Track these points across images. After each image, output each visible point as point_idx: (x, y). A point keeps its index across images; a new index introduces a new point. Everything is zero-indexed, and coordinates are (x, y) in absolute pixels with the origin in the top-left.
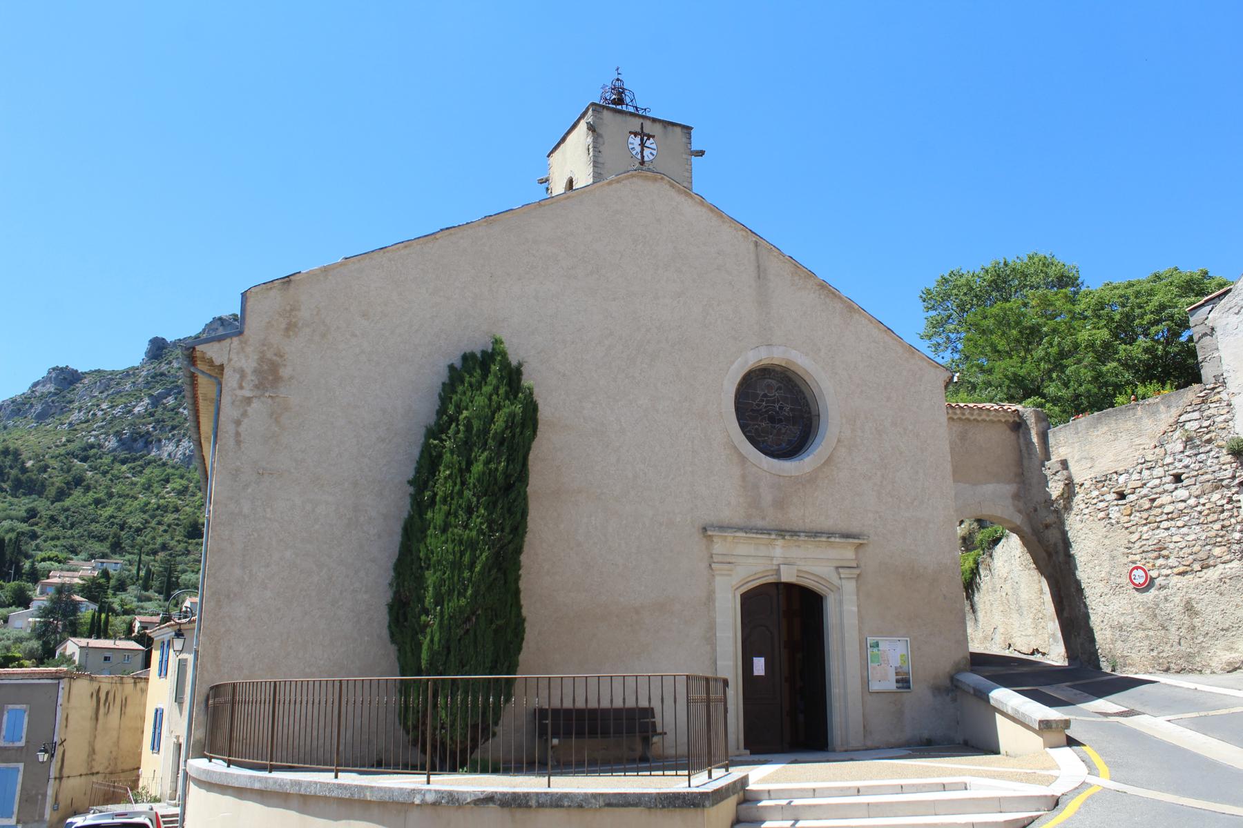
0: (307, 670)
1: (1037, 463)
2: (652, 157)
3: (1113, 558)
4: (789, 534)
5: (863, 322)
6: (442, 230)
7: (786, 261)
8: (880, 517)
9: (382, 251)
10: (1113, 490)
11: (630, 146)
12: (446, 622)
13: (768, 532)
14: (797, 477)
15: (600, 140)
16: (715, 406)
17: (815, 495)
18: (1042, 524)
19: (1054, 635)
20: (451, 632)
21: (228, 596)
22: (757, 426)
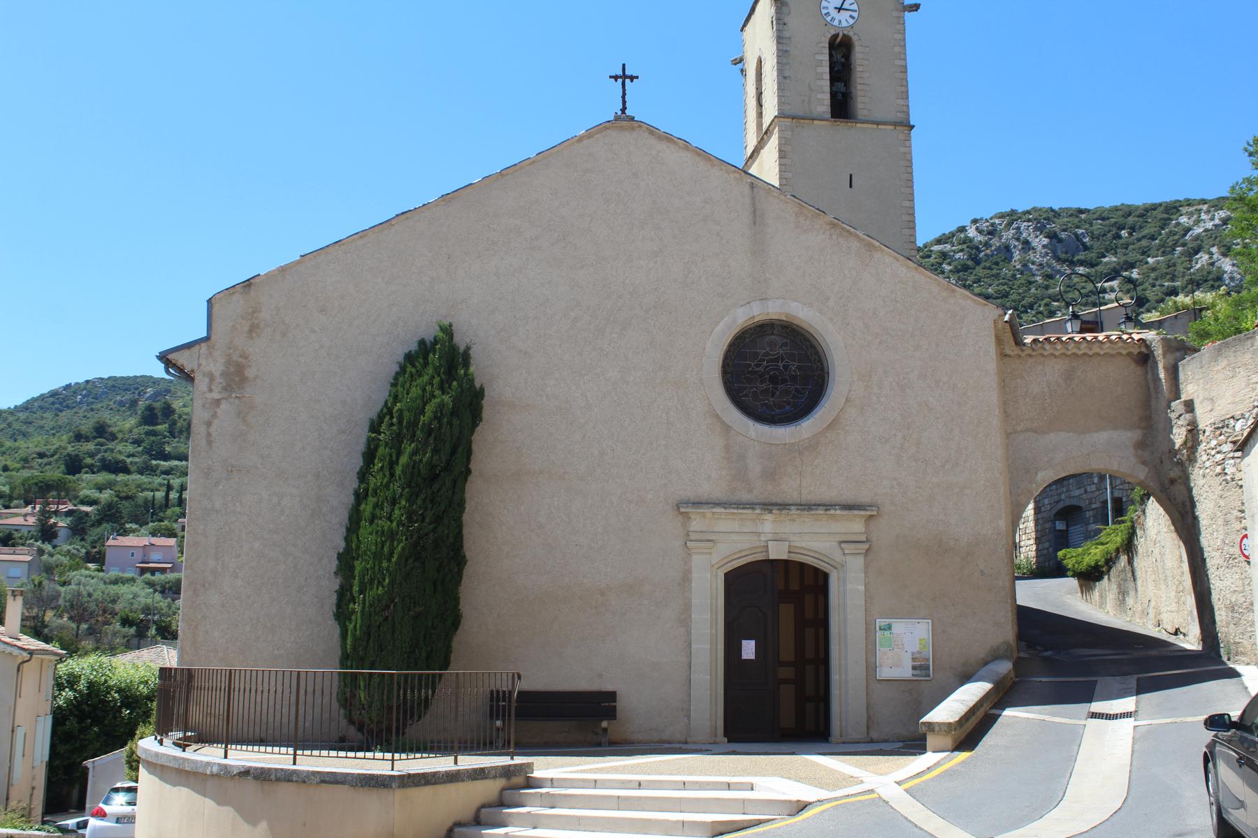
0: (276, 652)
1: (1164, 404)
2: (851, 21)
3: (1227, 523)
4: (778, 507)
5: (887, 260)
6: (397, 215)
7: (788, 200)
8: (899, 484)
9: (337, 245)
10: (1230, 439)
11: (824, 11)
12: (367, 609)
13: (751, 505)
14: (793, 445)
15: (785, 10)
16: (695, 373)
17: (815, 463)
18: (1167, 478)
19: (1191, 612)
20: (371, 621)
21: (204, 586)
22: (755, 389)
